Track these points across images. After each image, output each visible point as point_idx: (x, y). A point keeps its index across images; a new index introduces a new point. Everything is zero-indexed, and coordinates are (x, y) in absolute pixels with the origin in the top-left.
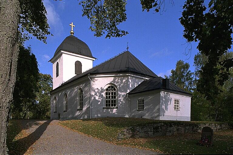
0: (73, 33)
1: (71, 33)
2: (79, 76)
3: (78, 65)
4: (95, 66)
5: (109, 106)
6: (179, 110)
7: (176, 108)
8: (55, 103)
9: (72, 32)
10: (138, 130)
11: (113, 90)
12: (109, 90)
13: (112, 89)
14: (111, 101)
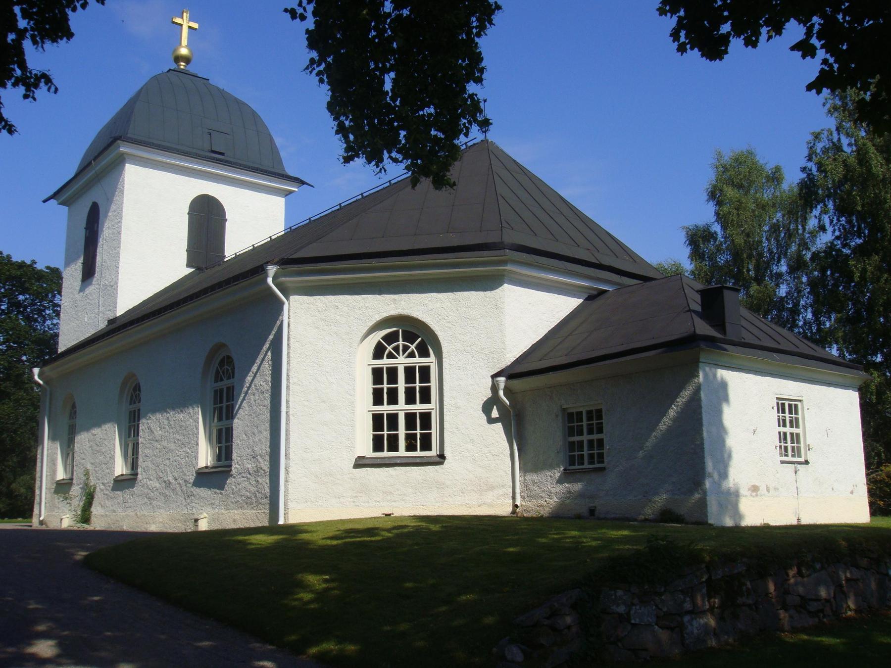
0: (187, 60)
1: (178, 59)
2: (214, 276)
3: (207, 219)
4: (301, 218)
5: (394, 447)
6: (807, 462)
7: (791, 446)
8: (579, 531)
9: (184, 51)
10: (622, 609)
11: (411, 355)
12: (391, 356)
13: (406, 348)
14: (402, 443)
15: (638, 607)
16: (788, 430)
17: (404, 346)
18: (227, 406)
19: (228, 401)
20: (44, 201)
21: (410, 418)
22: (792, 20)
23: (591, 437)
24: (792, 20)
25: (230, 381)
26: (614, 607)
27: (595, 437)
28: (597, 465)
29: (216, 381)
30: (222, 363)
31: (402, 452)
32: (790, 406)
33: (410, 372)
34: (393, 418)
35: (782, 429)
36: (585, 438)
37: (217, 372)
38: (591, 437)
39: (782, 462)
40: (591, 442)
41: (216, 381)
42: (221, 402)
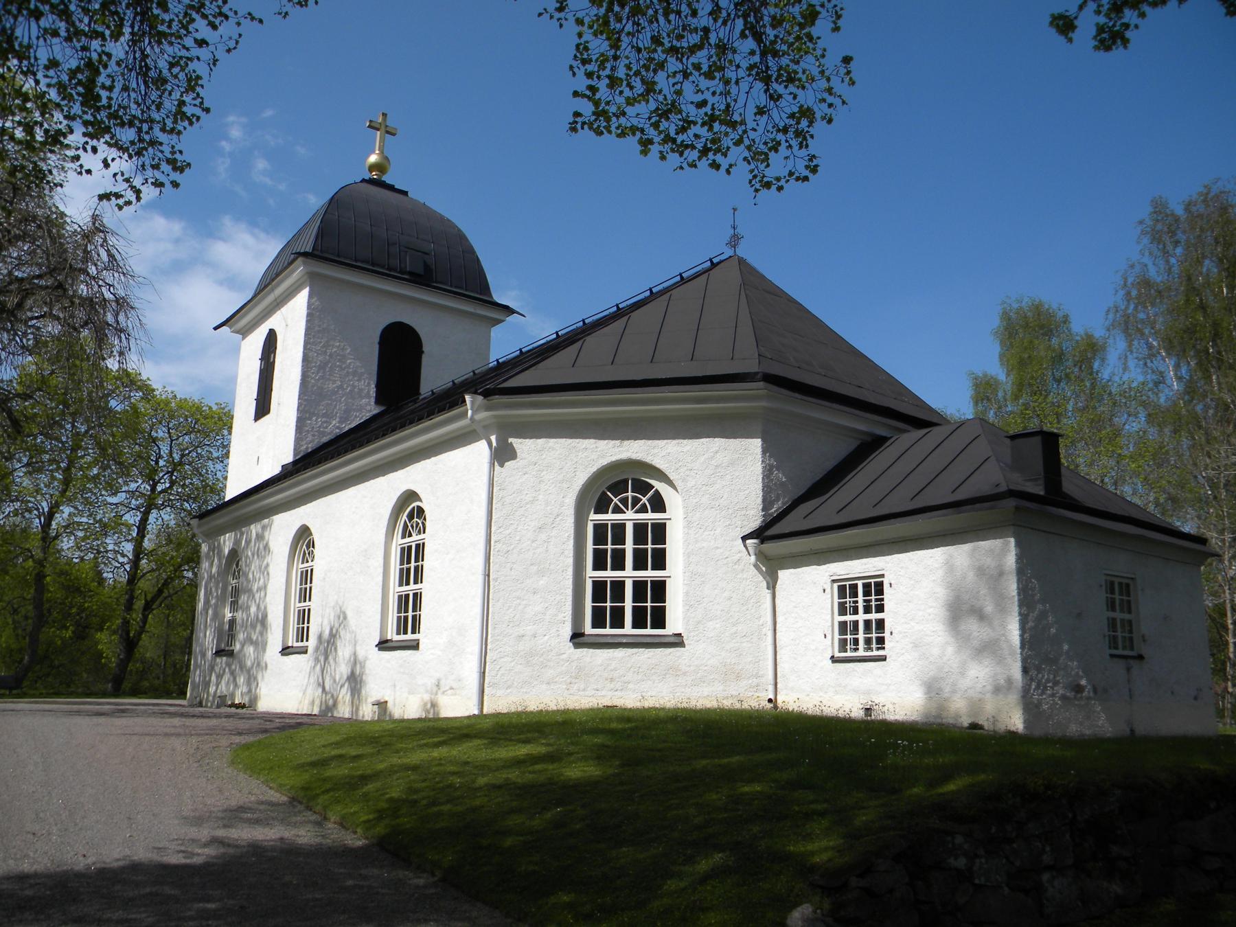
5: (618, 622)
10: (961, 863)
11: (643, 510)
12: (617, 510)
15: (983, 860)
16: (1118, 615)
17: (634, 498)
18: (416, 568)
19: (417, 560)
20: (215, 328)
21: (639, 586)
22: (756, 444)
23: (868, 617)
24: (756, 444)
25: (422, 536)
26: (952, 861)
27: (874, 616)
28: (875, 653)
29: (403, 537)
30: (411, 517)
31: (628, 629)
32: (1120, 584)
33: (640, 529)
34: (640, 564)
35: (1112, 614)
36: (861, 617)
37: (406, 526)
38: (868, 617)
39: (1112, 656)
40: (868, 623)
41: (403, 537)
42: (409, 562)
